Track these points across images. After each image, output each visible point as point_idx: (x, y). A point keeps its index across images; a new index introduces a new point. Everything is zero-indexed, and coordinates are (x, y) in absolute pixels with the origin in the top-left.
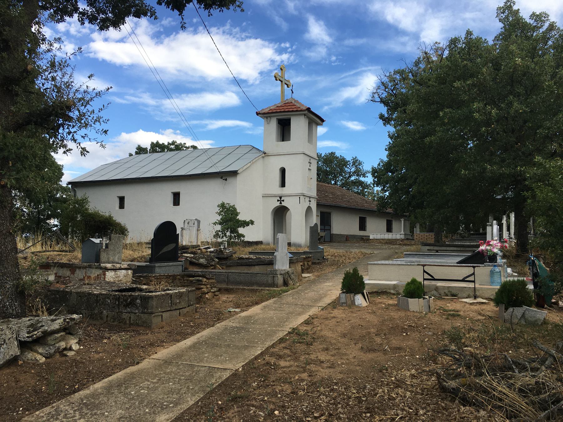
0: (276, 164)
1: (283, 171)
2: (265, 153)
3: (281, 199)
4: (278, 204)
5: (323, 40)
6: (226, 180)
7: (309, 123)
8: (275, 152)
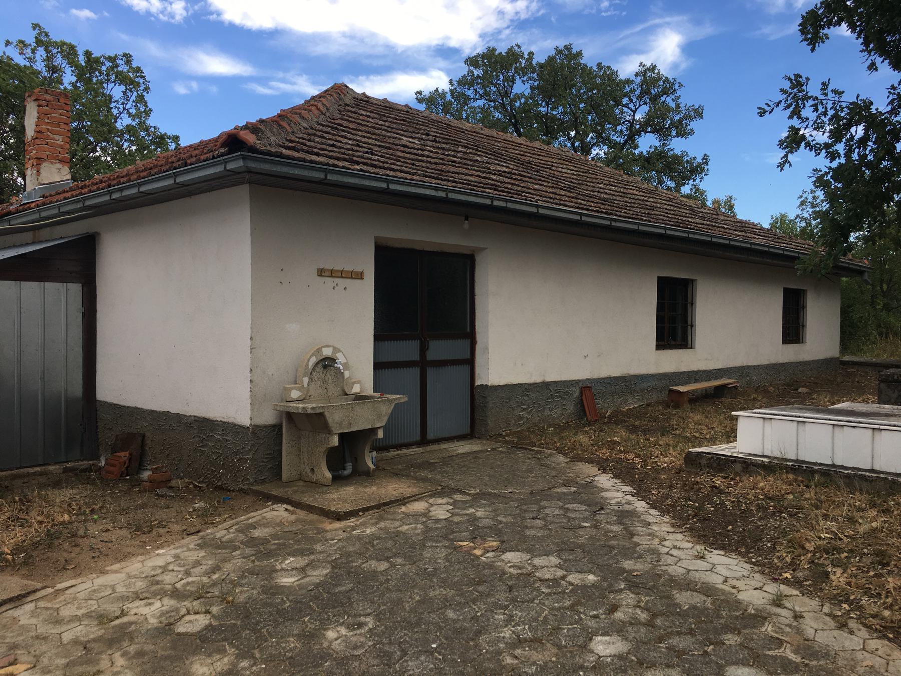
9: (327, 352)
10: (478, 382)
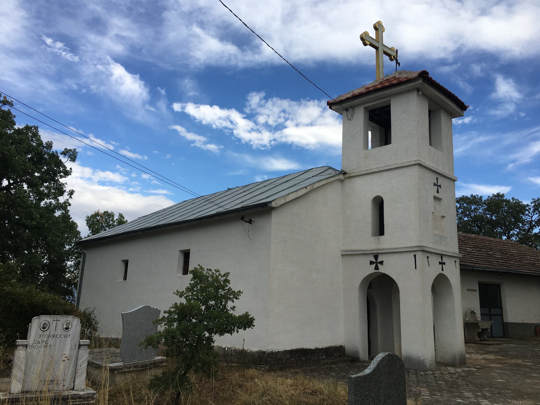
0: (365, 190)
1: (379, 204)
2: (345, 173)
3: (376, 259)
4: (371, 270)
5: (511, 97)
6: (250, 222)
7: (431, 113)
8: (363, 169)
9: (472, 309)
10: (504, 321)
